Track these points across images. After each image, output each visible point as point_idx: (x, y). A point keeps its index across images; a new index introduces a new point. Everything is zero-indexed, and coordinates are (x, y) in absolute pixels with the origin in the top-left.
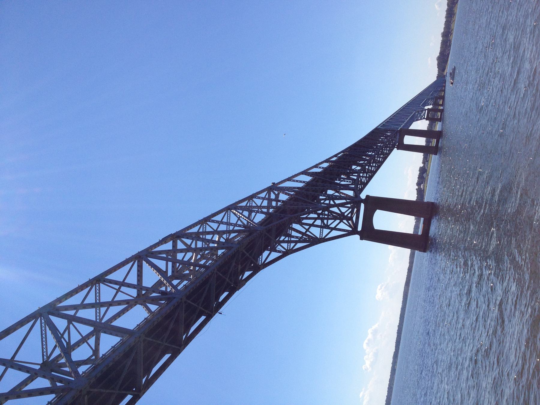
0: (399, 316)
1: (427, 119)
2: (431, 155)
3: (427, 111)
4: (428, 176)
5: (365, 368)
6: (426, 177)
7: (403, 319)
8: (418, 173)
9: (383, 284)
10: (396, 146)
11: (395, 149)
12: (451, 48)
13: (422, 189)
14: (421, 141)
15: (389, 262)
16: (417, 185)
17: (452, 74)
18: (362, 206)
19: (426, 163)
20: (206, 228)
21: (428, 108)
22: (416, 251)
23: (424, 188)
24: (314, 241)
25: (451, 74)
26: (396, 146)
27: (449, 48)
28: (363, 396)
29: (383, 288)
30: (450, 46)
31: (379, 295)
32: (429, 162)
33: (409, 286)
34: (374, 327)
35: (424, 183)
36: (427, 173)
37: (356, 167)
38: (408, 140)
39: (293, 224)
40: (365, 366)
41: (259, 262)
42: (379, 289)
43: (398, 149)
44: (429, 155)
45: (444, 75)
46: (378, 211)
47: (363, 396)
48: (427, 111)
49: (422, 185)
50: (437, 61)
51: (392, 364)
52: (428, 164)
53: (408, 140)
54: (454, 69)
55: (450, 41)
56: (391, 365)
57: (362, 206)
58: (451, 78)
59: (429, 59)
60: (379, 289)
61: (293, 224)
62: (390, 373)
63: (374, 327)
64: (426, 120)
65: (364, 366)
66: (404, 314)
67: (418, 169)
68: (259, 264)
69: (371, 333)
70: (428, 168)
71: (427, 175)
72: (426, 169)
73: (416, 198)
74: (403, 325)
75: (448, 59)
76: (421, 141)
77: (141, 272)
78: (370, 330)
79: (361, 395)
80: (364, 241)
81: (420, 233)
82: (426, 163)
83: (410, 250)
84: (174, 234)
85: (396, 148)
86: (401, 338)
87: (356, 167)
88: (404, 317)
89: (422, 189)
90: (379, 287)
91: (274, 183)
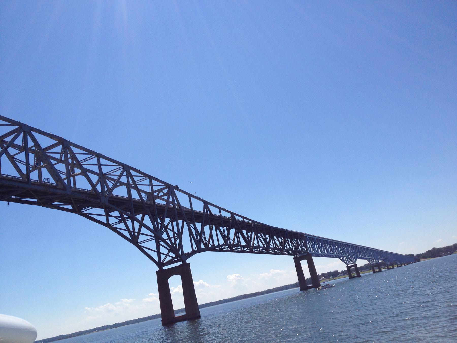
0: (218, 300)
1: (347, 267)
2: (348, 276)
3: (354, 264)
4: (332, 280)
5: (172, 289)
6: (331, 279)
7: (218, 304)
8: (332, 270)
9: (241, 277)
10: (296, 256)
11: (293, 257)
12: (443, 257)
13: (320, 280)
14: (307, 275)
15: (261, 275)
16: (322, 274)
17: (327, 286)
18: (180, 263)
19: (342, 274)
20: (87, 158)
21: (357, 265)
22: (161, 318)
23: (322, 280)
24: (134, 240)
25: (327, 285)
26: (296, 256)
27: (446, 255)
28: (152, 296)
29: (238, 278)
30: (448, 254)
31: (232, 277)
32: (344, 276)
33: (243, 299)
34: (205, 283)
35: (325, 279)
36: (335, 278)
37: (232, 240)
38: (304, 264)
39: (131, 220)
40: (173, 288)
41: (83, 209)
42: (236, 276)
43: (294, 258)
44: (348, 275)
45: (420, 260)
46: (180, 276)
47: (152, 296)
48: (354, 264)
49: (324, 278)
50: (432, 249)
51: (116, 323)
52: (342, 276)
53: (304, 264)
54: (332, 286)
55: (452, 253)
56: (180, 309)
57: (180, 263)
58: (324, 286)
59: (440, 240)
60: (236, 276)
61: (131, 220)
62: (138, 318)
63: (205, 283)
64: (346, 267)
65: (173, 288)
66: (221, 303)
67: (335, 270)
68: (82, 210)
69: (200, 283)
70: (339, 277)
71: (333, 278)
72: (338, 276)
73: (359, 267)
74: (212, 306)
75: (436, 257)
76: (307, 275)
77: (11, 134)
78: (202, 281)
79: (151, 294)
80: (155, 276)
81: (176, 315)
82: (342, 274)
83: (161, 313)
84: (65, 140)
85: (295, 256)
86: (202, 308)
87: (232, 240)
88: (219, 304)
89: (320, 280)
90: (237, 275)
91: (177, 187)
